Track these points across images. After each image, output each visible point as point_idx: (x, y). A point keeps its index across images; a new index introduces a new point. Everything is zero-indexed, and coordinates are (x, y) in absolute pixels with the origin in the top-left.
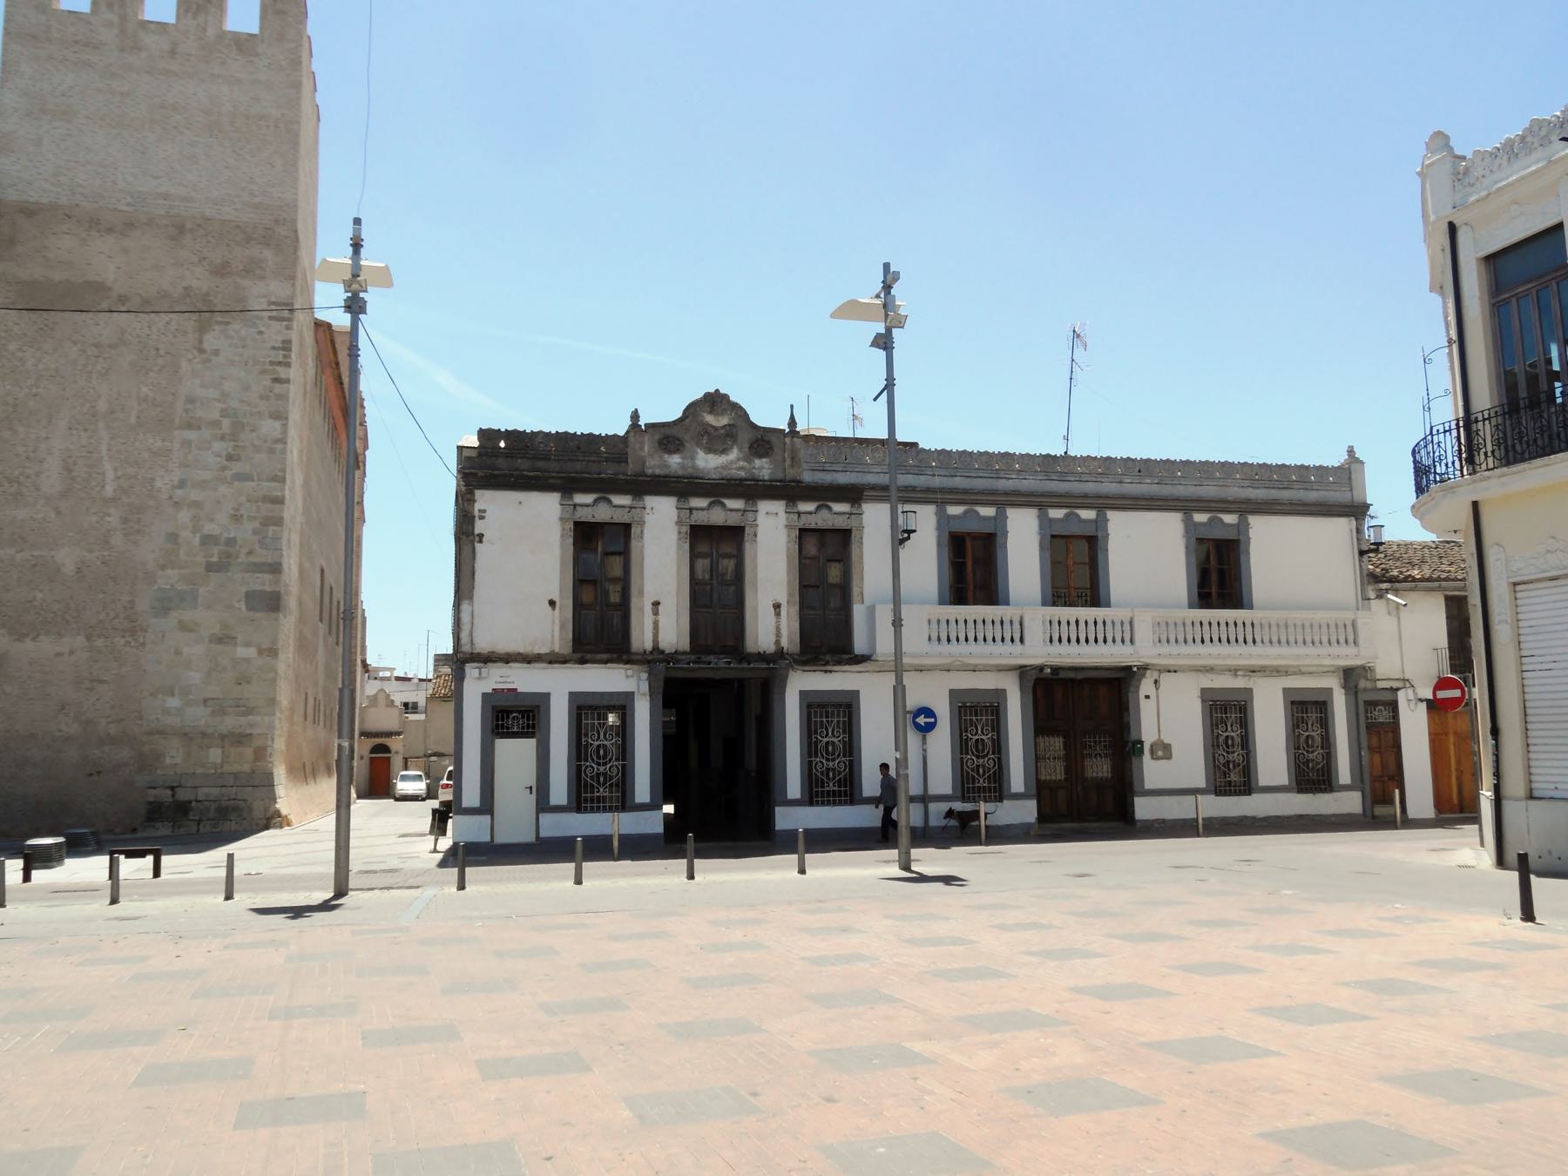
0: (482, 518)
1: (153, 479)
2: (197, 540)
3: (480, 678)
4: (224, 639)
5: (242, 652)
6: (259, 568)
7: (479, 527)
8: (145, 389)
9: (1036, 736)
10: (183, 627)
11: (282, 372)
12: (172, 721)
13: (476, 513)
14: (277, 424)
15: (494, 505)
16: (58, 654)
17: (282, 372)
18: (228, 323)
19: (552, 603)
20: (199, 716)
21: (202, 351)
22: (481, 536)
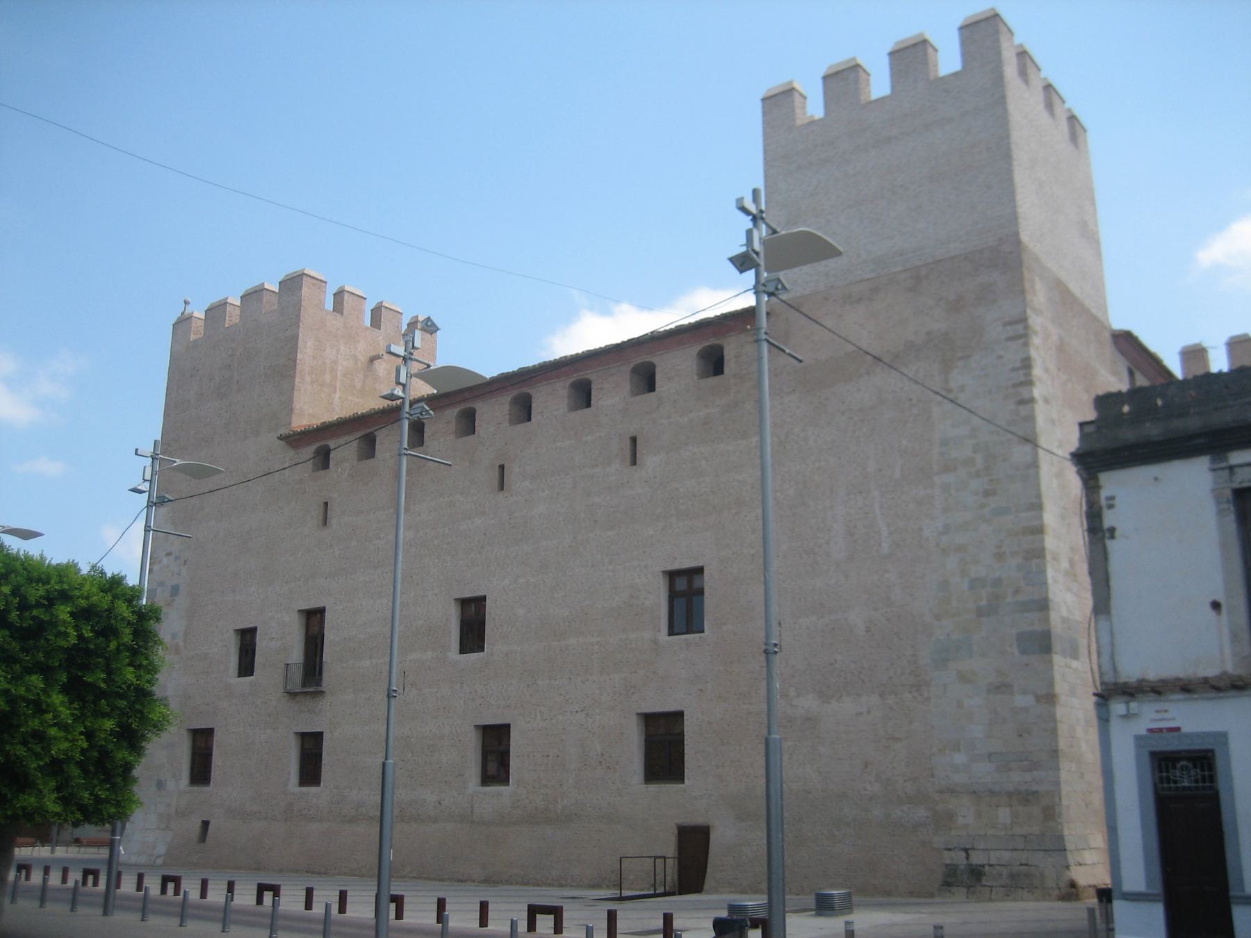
0: (1111, 507)
1: (921, 529)
3: (1127, 716)
4: (1001, 688)
5: (1021, 700)
6: (1025, 607)
7: (1109, 519)
10: (963, 678)
11: (1024, 392)
13: (1103, 502)
14: (1028, 448)
15: (1127, 489)
16: (859, 714)
17: (1024, 392)
18: (969, 356)
19: (1216, 606)
20: (984, 772)
22: (1112, 530)
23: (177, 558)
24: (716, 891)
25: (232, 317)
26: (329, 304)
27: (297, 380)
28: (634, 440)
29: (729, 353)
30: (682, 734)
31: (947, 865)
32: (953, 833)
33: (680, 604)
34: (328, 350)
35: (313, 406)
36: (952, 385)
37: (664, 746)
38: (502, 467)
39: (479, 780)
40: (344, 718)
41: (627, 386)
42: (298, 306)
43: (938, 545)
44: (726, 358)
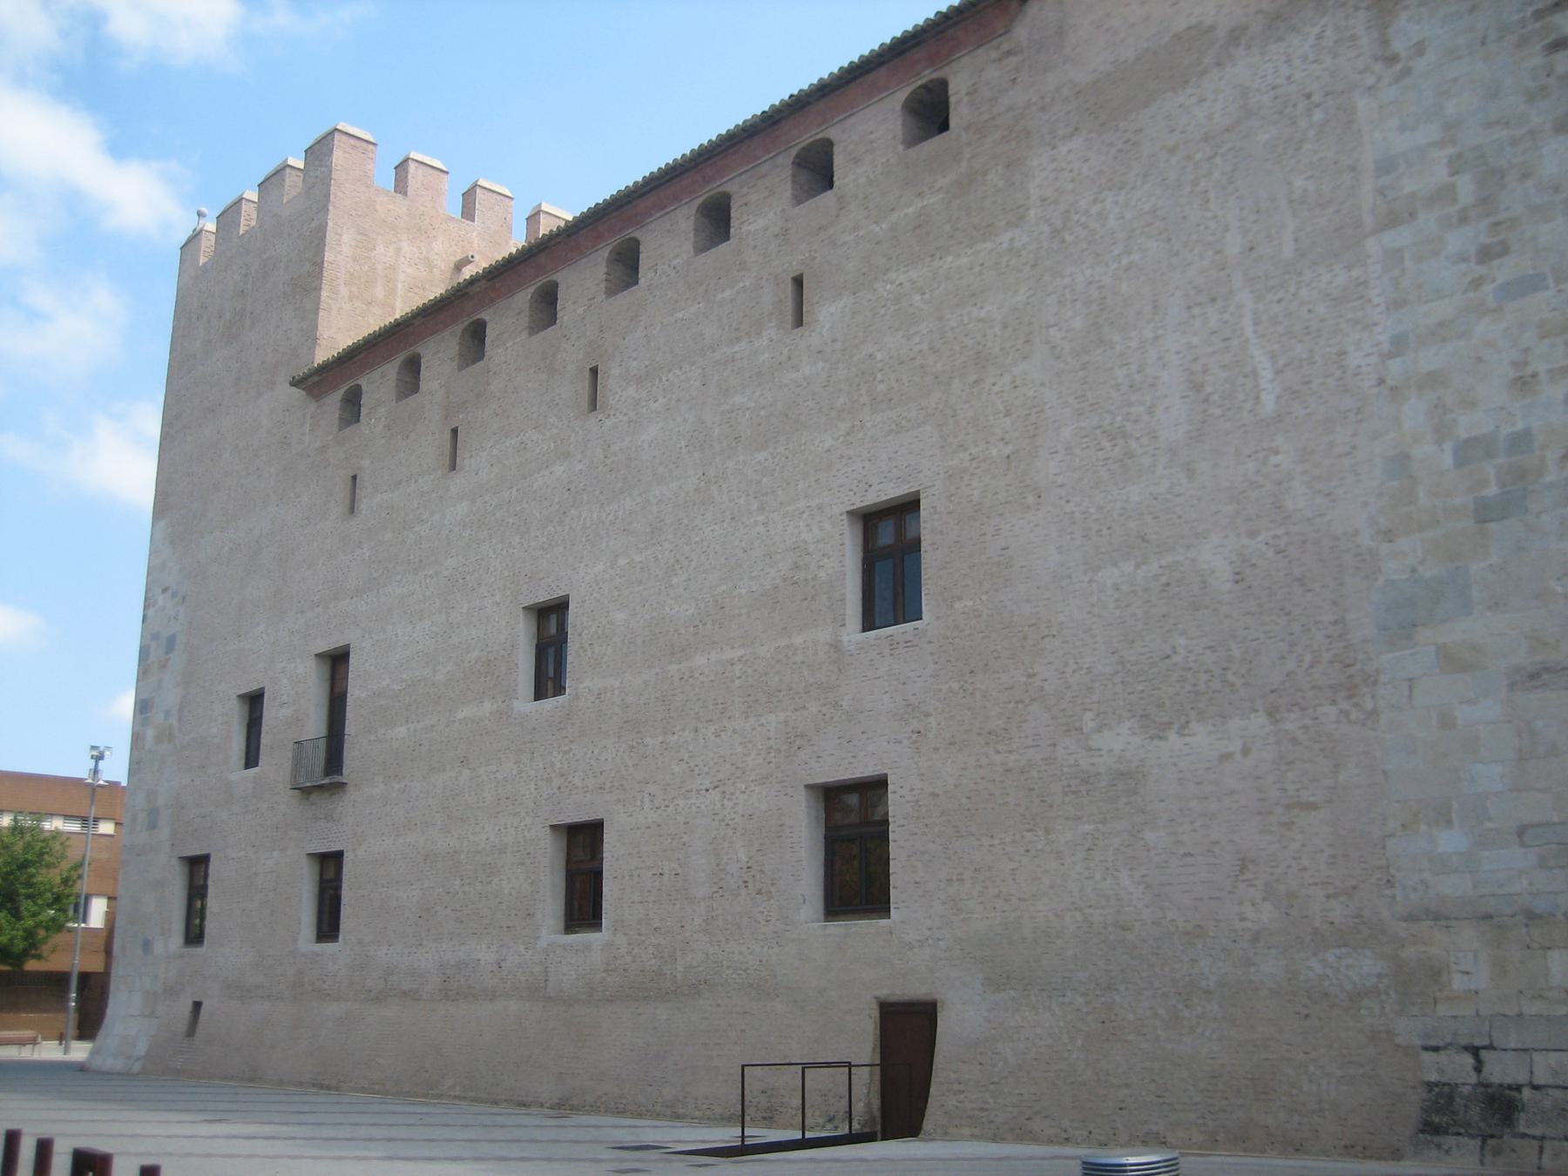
1: (1342, 353)
2: (1448, 460)
8: (1299, 182)
9: (106, 974)
10: (1451, 661)
12: (1452, 886)
16: (1226, 757)
20: (1512, 871)
21: (1392, 59)
23: (174, 595)
24: (945, 1135)
25: (248, 218)
26: (387, 179)
27: (324, 294)
28: (798, 282)
29: (958, 88)
30: (886, 823)
31: (1430, 1086)
32: (1442, 1010)
33: (884, 570)
34: (380, 249)
35: (341, 326)
36: (1398, 46)
37: (855, 851)
38: (594, 371)
39: (562, 924)
40: (365, 826)
41: (786, 191)
42: (326, 181)
43: (1381, 381)
44: (952, 100)
